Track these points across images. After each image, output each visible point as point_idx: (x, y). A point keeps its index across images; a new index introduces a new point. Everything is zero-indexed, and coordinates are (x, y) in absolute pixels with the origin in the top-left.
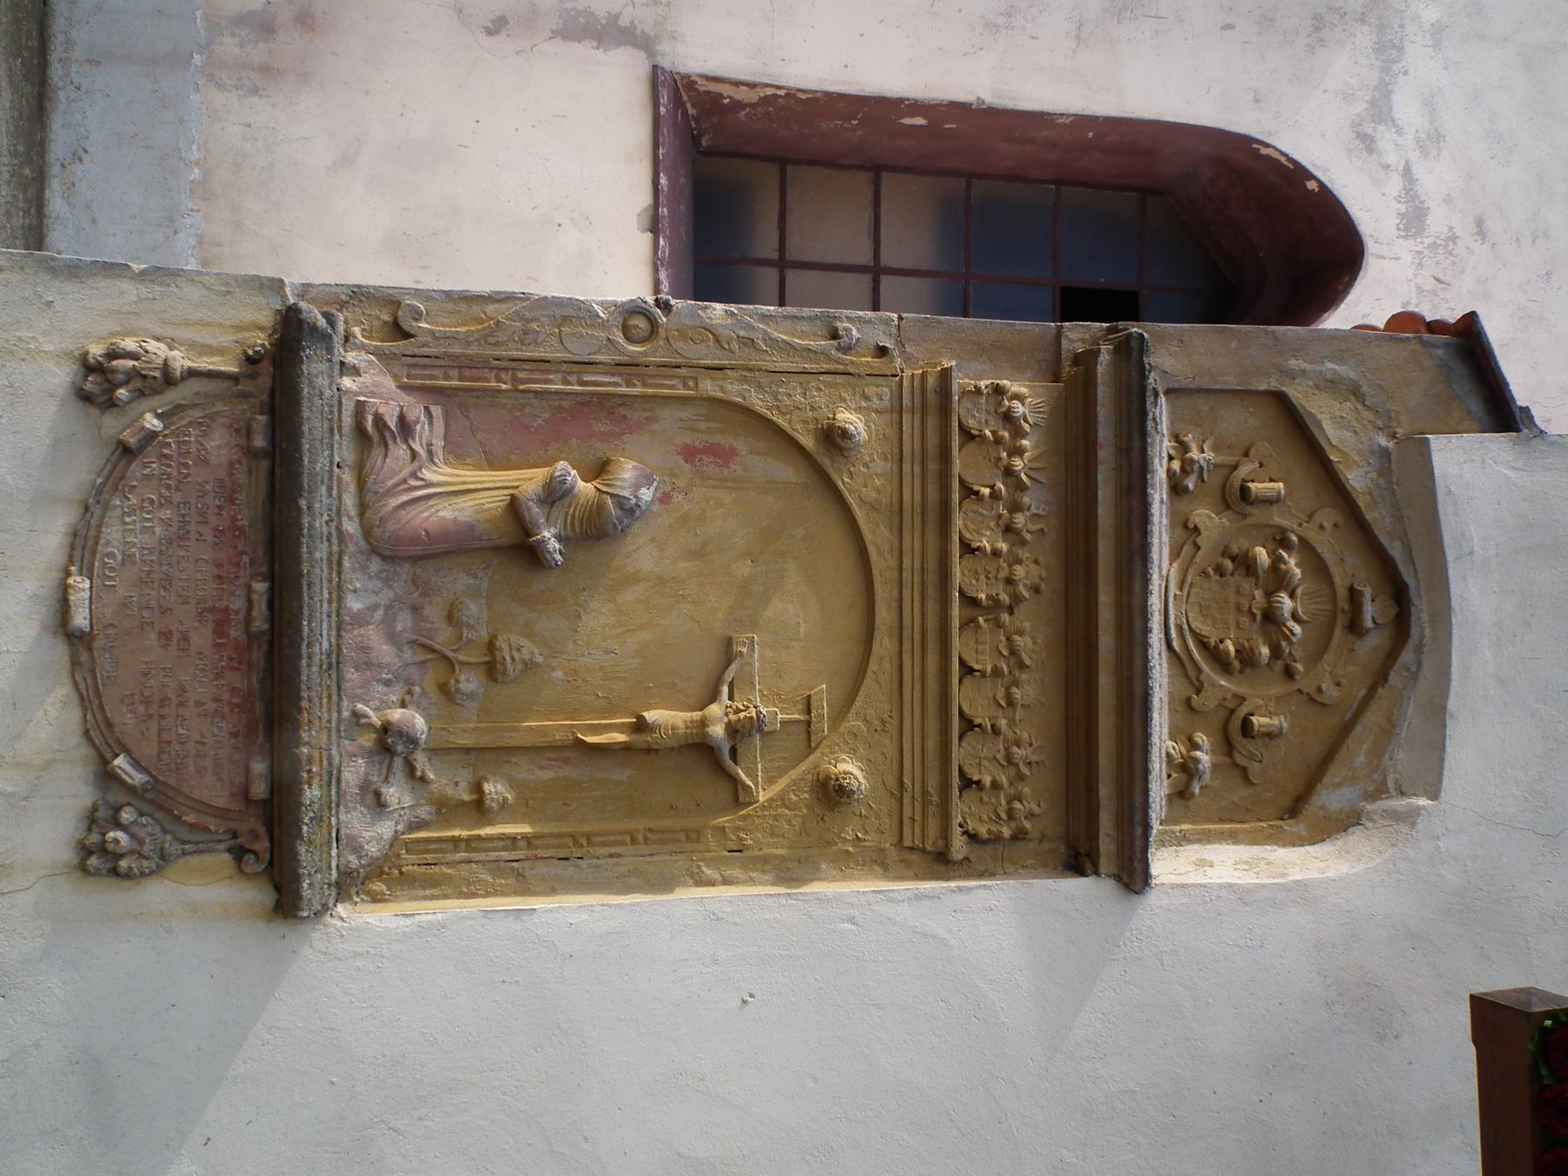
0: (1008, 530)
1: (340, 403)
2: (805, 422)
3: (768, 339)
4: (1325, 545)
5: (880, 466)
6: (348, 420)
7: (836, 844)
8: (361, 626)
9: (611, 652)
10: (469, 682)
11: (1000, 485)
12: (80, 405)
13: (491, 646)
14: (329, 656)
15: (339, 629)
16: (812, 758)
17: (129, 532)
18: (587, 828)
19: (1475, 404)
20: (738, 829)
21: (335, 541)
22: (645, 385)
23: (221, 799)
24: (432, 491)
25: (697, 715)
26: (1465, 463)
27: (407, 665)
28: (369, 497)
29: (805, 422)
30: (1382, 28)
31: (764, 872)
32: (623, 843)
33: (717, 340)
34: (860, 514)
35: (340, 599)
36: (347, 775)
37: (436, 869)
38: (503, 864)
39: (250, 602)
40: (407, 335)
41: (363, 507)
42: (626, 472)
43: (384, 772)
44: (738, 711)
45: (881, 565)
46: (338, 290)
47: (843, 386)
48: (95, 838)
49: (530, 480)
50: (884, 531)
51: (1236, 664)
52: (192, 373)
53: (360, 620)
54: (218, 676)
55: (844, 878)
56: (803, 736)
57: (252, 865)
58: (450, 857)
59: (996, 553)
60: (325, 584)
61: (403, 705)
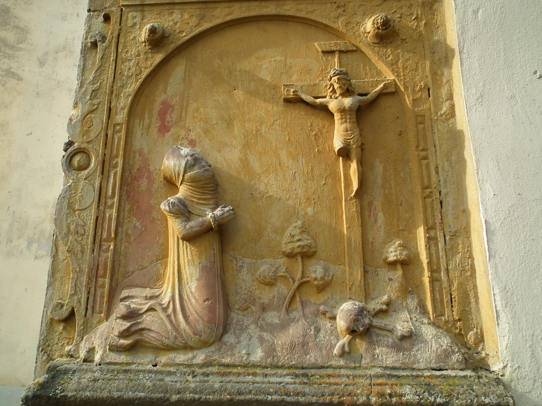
1: (110, 363)
2: (147, 59)
3: (93, 82)
5: (177, 16)
6: (122, 358)
7: (420, 32)
8: (275, 350)
9: (293, 173)
10: (316, 271)
13: (291, 256)
14: (297, 376)
15: (277, 367)
16: (364, 49)
18: (418, 189)
20: (414, 91)
21: (210, 369)
22: (117, 156)
24: (177, 297)
25: (337, 116)
27: (304, 315)
28: (179, 342)
29: (147, 59)
31: (442, 74)
32: (428, 165)
33: (91, 112)
34: (206, 26)
35: (254, 366)
36: (389, 362)
37: (455, 294)
38: (448, 247)
40: (72, 314)
41: (186, 348)
42: (172, 163)
43: (384, 333)
44: (334, 91)
46: (39, 361)
47: (126, 38)
49: (175, 227)
50: (217, 12)
53: (271, 351)
55: (443, 25)
56: (349, 55)
58: (445, 284)
60: (241, 379)
61: (334, 318)
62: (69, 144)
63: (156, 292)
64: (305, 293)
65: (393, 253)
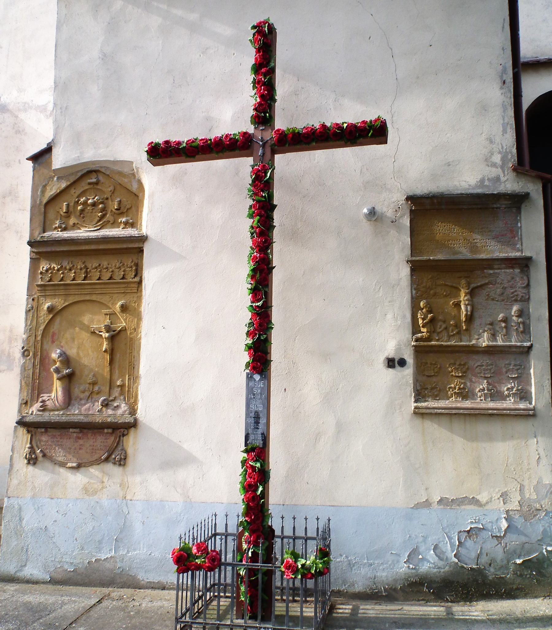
0: (70, 270)
2: (47, 317)
4: (78, 192)
6: (41, 413)
10: (96, 388)
11: (61, 272)
12: (36, 465)
13: (90, 384)
17: (60, 455)
18: (127, 362)
19: (47, 156)
23: (112, 438)
26: (60, 159)
28: (56, 408)
29: (47, 317)
30: (19, 110)
33: (30, 336)
34: (67, 304)
39: (74, 432)
40: (27, 402)
41: (58, 410)
45: (77, 299)
48: (117, 463)
49: (55, 376)
51: (104, 213)
52: (31, 443)
53: (80, 411)
54: (88, 439)
57: (126, 432)
59: (75, 273)
62: (23, 348)
63: (50, 395)
64: (91, 396)
65: (119, 383)
